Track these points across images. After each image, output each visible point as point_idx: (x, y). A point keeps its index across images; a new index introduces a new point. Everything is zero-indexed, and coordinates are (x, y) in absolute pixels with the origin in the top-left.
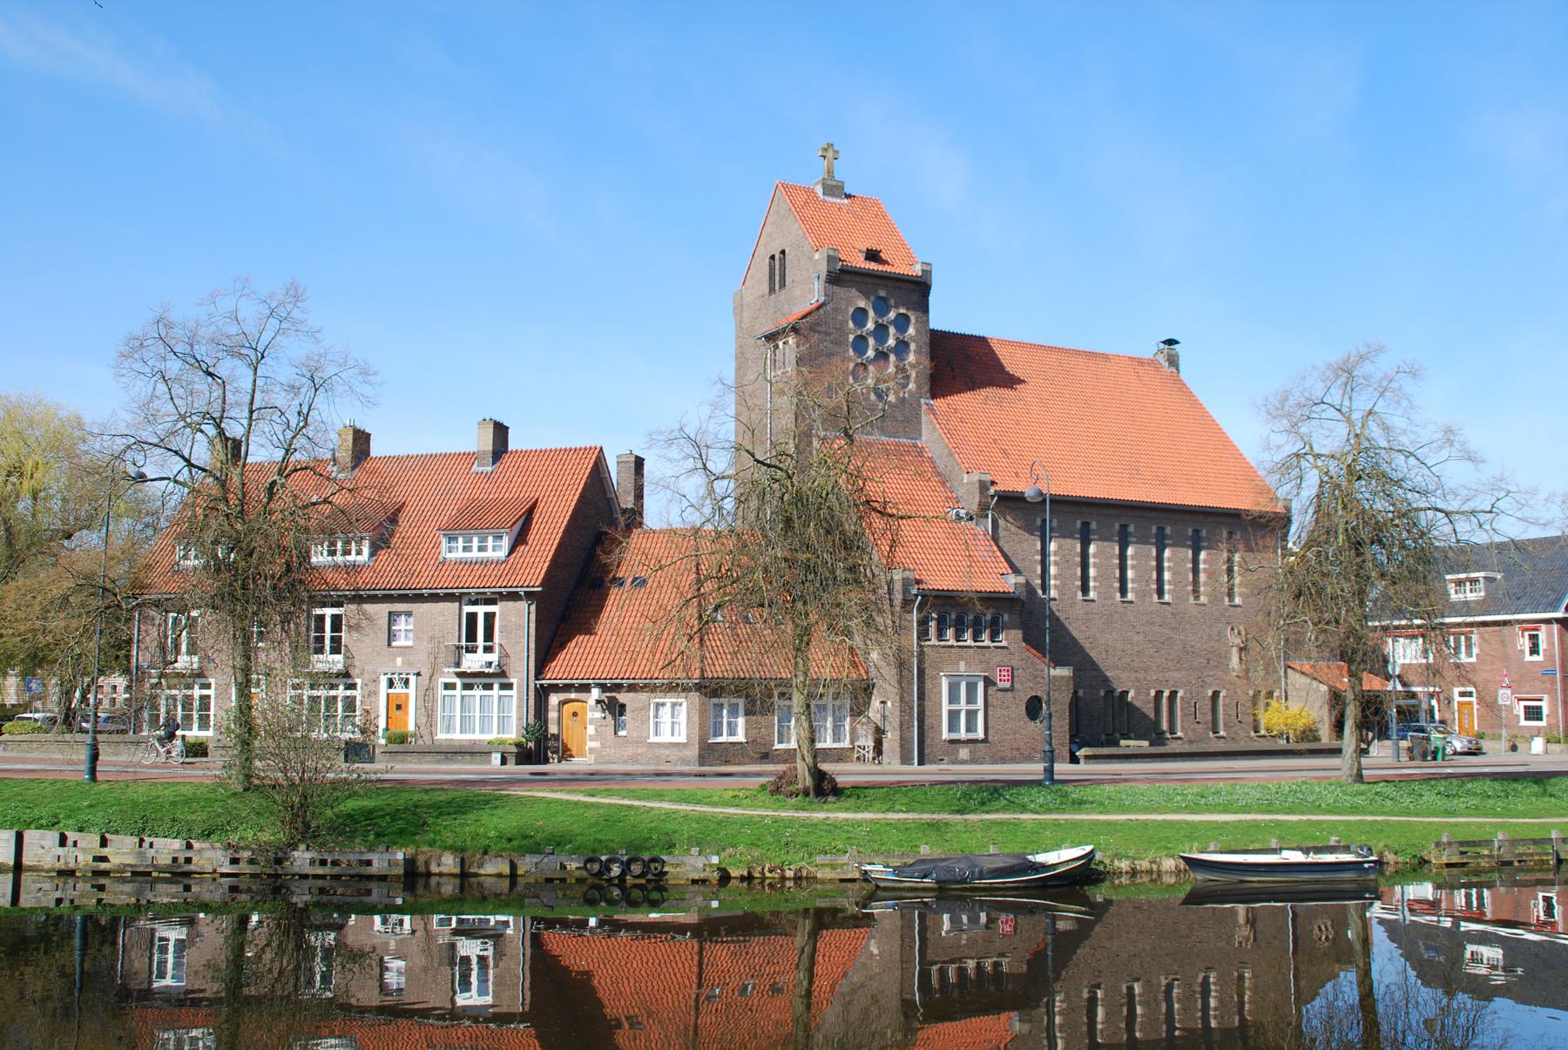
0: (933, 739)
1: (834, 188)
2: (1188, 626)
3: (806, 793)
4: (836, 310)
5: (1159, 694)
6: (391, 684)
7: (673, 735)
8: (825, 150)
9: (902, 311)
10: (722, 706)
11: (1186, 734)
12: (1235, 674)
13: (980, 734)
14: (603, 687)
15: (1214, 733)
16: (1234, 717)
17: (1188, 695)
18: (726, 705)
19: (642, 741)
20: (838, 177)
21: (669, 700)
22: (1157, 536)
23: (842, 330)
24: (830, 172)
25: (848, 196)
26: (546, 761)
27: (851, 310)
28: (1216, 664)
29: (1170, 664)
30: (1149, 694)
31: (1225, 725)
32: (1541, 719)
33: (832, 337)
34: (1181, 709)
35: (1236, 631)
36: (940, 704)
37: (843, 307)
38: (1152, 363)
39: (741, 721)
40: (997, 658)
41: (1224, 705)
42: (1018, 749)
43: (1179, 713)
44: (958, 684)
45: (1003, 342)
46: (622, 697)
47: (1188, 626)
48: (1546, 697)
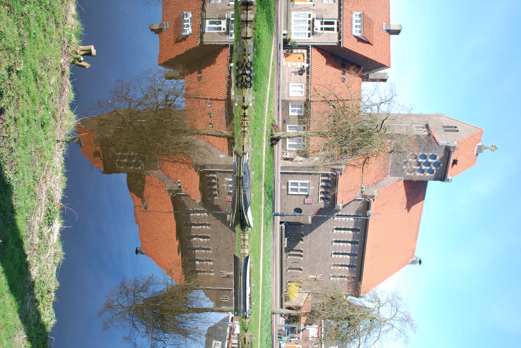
1: (480, 149)
5: (302, 251)
9: (435, 172)
11: (288, 259)
13: (290, 193)
14: (308, 68)
17: (301, 261)
18: (301, 109)
20: (485, 151)
24: (486, 148)
25: (477, 154)
26: (284, 49)
27: (436, 154)
29: (311, 255)
30: (302, 248)
31: (291, 272)
33: (426, 147)
35: (322, 277)
37: (437, 151)
39: (296, 114)
41: (297, 272)
46: (305, 74)
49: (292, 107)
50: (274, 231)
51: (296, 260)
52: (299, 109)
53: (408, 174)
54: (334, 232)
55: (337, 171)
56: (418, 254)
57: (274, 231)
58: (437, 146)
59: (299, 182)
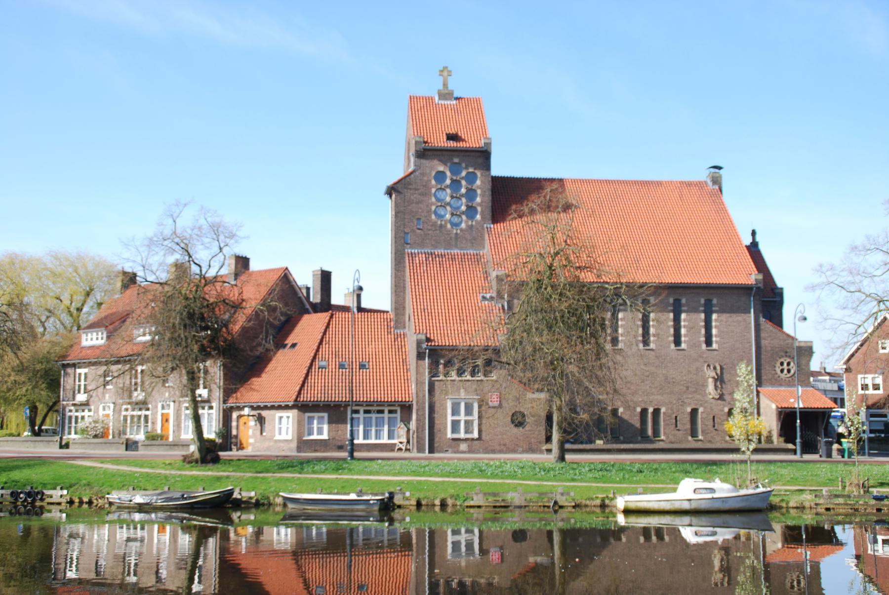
0: (440, 438)
1: (446, 95)
2: (669, 365)
3: (197, 462)
4: (423, 174)
5: (644, 411)
6: (163, 408)
7: (287, 434)
8: (442, 71)
9: (471, 170)
10: (313, 418)
11: (668, 437)
12: (711, 397)
13: (476, 435)
14: (253, 408)
15: (692, 437)
16: (711, 427)
17: (670, 411)
18: (316, 417)
19: (271, 439)
20: (450, 87)
21: (316, 415)
22: (674, 305)
23: (427, 186)
24: (445, 85)
25: (457, 99)
26: (231, 450)
27: (433, 173)
28: (694, 390)
29: (653, 390)
30: (635, 411)
31: (702, 432)
33: (420, 191)
34: (664, 421)
35: (712, 367)
36: (446, 416)
37: (428, 172)
38: (700, 185)
39: (326, 427)
41: (702, 418)
42: (504, 445)
43: (662, 423)
44: (459, 404)
45: (574, 181)
46: (264, 413)
47: (669, 365)
49: (371, 439)
50: (378, 459)
51: (668, 422)
52: (315, 422)
53: (478, 217)
54: (686, 348)
55: (421, 347)
56: (702, 175)
57: (378, 459)
58: (417, 173)
59: (450, 418)
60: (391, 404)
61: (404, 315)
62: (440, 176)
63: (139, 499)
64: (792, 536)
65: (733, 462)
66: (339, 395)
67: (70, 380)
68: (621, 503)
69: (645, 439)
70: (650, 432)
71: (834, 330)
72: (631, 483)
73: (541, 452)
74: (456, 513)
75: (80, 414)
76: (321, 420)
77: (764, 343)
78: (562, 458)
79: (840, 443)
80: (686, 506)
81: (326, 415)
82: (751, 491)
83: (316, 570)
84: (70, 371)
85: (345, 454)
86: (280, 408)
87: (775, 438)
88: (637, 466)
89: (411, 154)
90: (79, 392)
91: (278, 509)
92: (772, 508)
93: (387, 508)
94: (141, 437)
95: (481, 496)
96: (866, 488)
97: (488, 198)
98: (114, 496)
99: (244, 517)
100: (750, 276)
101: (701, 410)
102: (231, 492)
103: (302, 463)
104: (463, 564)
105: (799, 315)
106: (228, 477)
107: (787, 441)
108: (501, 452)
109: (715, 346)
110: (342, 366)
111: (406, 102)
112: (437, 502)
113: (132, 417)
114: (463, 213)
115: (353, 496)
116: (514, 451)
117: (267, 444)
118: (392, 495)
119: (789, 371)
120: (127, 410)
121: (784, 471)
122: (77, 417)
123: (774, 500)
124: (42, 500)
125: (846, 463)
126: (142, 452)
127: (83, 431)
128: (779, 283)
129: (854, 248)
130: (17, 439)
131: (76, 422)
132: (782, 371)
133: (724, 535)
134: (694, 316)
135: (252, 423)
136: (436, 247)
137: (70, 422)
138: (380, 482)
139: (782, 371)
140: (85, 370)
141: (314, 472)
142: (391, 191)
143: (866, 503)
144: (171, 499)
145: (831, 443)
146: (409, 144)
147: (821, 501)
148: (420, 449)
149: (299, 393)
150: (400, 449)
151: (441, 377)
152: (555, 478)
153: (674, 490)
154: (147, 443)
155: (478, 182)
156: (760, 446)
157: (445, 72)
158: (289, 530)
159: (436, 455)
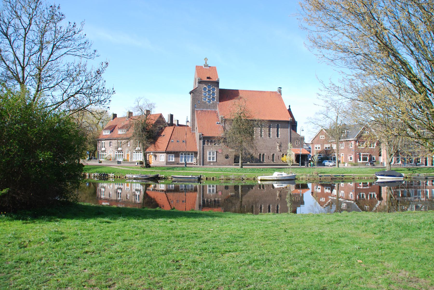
1: (206, 65)
5: (260, 154)
6: (127, 152)
9: (213, 87)
13: (215, 161)
14: (153, 153)
21: (171, 155)
23: (201, 91)
24: (206, 63)
25: (209, 67)
32: (367, 161)
38: (276, 92)
39: (174, 158)
40: (219, 148)
44: (211, 152)
45: (241, 90)
48: (352, 155)
53: (215, 100)
56: (276, 90)
60: (192, 152)
61: (194, 127)
62: (205, 89)
63: (134, 177)
64: (298, 187)
65: (287, 168)
66: (177, 150)
67: (100, 144)
68: (259, 178)
69: (260, 162)
70: (262, 160)
71: (311, 134)
72: (260, 173)
73: (233, 165)
74: (216, 181)
75: (103, 154)
76: (172, 156)
77: (292, 136)
78: (242, 167)
79: (310, 163)
80: (276, 179)
81: (174, 155)
82: (291, 175)
83: (170, 195)
84: (100, 141)
85: (184, 166)
86: (161, 153)
87: (294, 162)
88: (262, 169)
89: (196, 82)
90: (103, 147)
91: (170, 179)
92: (296, 179)
93: (199, 179)
94: (121, 160)
95: (223, 177)
96: (318, 174)
97: (218, 95)
98: (128, 176)
99: (161, 181)
100: (289, 119)
101: (275, 154)
102: (158, 175)
103: (173, 168)
104: (211, 195)
105: (302, 129)
106: (154, 171)
107: (297, 163)
108: (222, 165)
109: (279, 137)
110: (178, 142)
111: (195, 68)
112: (212, 178)
113: (118, 155)
114: (211, 99)
115: (190, 176)
116: (225, 165)
117: (157, 163)
118: (201, 176)
119: (298, 144)
120: (116, 153)
121: (298, 170)
122: (104, 155)
123: (296, 177)
124: (107, 176)
125: (313, 168)
126: (122, 164)
127: (106, 158)
128: (296, 121)
129: (316, 113)
130: (110, 161)
131: (102, 156)
132: (296, 144)
133: (284, 186)
134: (274, 129)
135: (153, 157)
136: (204, 109)
137: (100, 156)
138: (196, 173)
139: (296, 144)
140: (104, 142)
141: (177, 170)
142: (190, 93)
143: (317, 178)
144: (143, 177)
145: (308, 163)
146: (196, 79)
147: (307, 177)
148: (200, 165)
149: (166, 149)
150: (194, 164)
151: (206, 145)
152: (241, 172)
153: (272, 175)
154: (123, 162)
155: (215, 91)
156: (293, 164)
157: (206, 59)
158: (164, 185)
159: (204, 166)
